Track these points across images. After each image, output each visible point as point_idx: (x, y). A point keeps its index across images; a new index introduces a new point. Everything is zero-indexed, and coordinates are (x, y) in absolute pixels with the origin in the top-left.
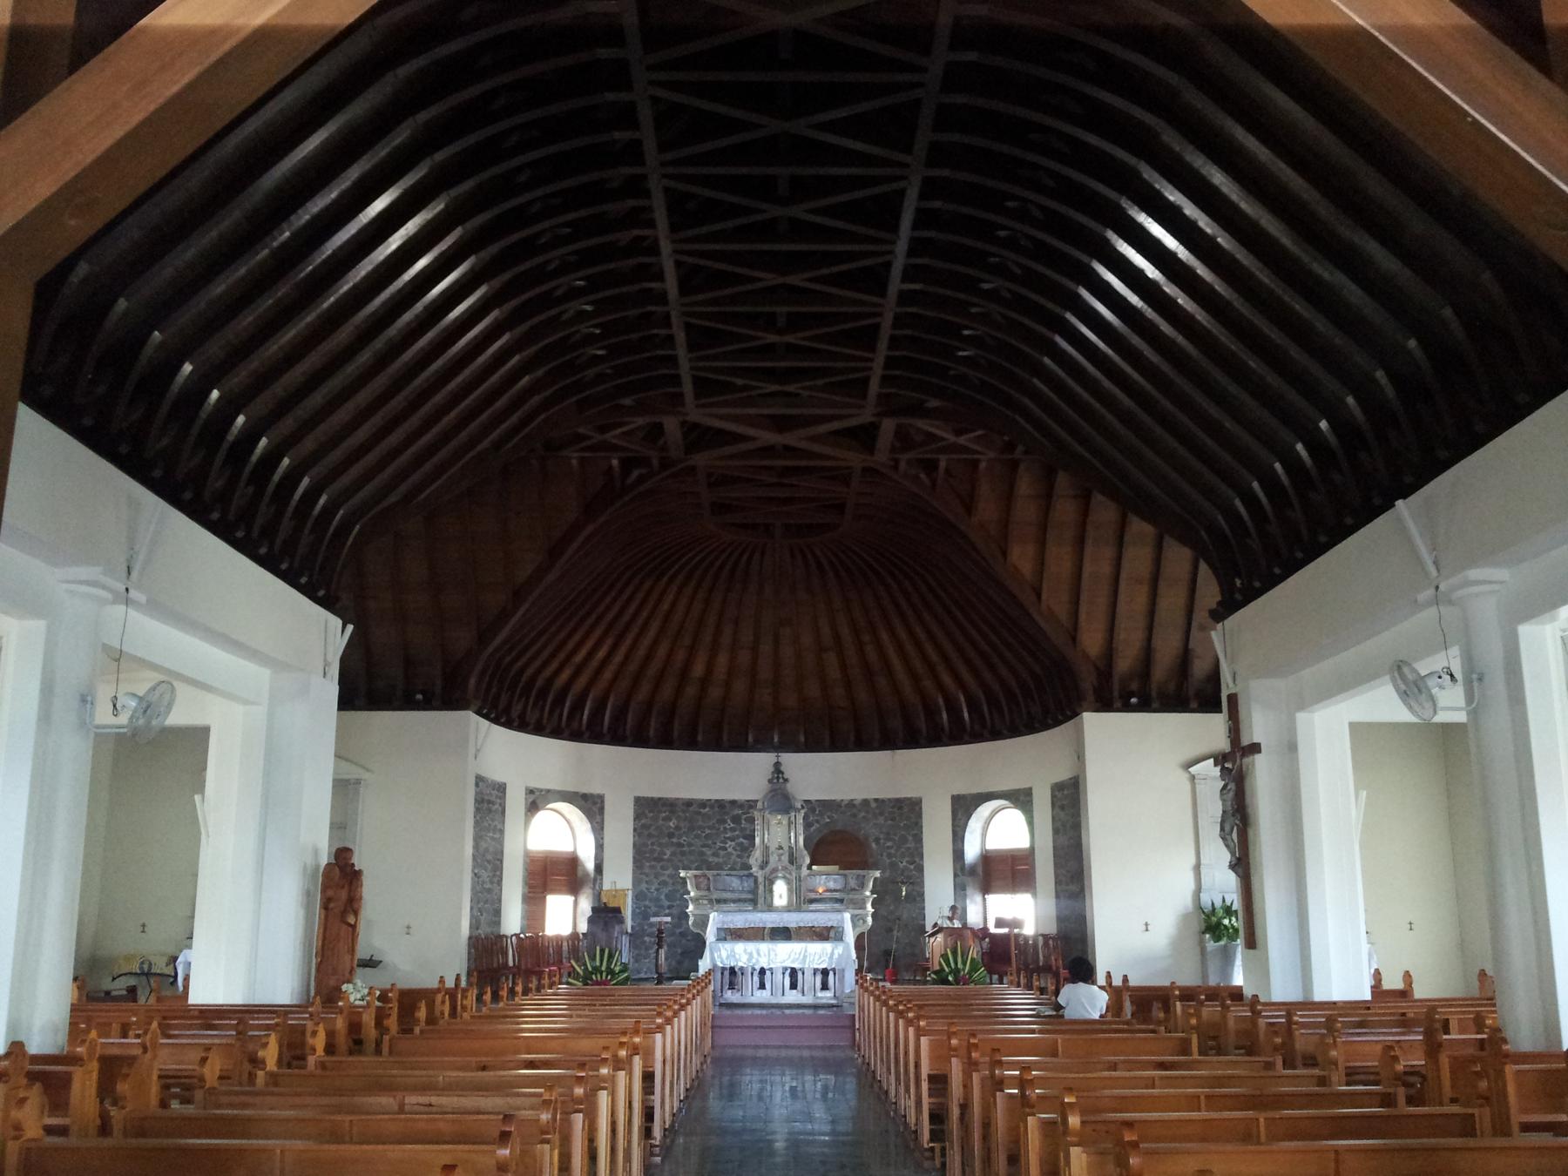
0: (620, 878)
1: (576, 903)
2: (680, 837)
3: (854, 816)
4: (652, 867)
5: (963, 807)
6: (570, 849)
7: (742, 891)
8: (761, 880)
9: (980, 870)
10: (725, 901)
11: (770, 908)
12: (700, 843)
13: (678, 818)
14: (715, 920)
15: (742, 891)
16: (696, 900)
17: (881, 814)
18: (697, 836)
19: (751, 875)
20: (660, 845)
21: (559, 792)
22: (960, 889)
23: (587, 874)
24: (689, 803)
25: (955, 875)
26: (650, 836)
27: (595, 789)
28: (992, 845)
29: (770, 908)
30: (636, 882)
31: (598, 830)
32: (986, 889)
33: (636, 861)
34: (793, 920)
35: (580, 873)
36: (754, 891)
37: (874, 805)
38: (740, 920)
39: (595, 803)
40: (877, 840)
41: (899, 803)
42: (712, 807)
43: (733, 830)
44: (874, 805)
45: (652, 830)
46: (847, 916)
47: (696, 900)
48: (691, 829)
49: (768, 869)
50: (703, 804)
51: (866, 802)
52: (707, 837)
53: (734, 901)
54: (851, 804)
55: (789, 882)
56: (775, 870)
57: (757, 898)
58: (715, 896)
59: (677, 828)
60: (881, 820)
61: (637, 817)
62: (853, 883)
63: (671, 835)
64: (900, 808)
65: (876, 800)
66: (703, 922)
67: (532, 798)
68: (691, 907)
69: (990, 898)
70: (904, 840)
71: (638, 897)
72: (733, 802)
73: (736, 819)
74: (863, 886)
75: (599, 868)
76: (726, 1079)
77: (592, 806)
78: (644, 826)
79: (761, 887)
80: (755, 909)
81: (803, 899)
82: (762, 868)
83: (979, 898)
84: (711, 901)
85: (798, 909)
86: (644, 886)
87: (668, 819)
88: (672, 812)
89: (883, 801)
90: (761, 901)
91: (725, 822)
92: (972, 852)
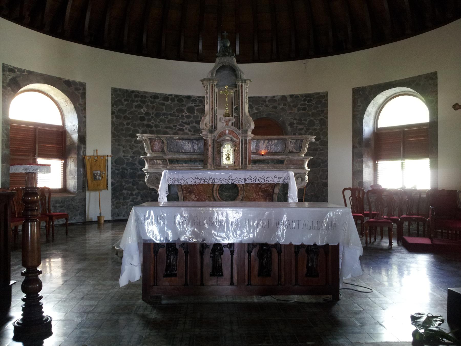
0: (101, 145)
1: (65, 166)
2: (149, 120)
3: (275, 107)
4: (127, 141)
5: (362, 97)
6: (60, 124)
7: (193, 153)
8: (210, 142)
9: (372, 143)
10: (178, 161)
11: (218, 166)
12: (164, 126)
13: (147, 106)
14: (166, 179)
15: (193, 153)
16: (150, 160)
17: (295, 106)
18: (161, 120)
19: (200, 139)
20: (134, 125)
21: (41, 75)
22: (358, 158)
23: (73, 143)
24: (155, 96)
25: (354, 147)
26: (125, 118)
27: (78, 79)
28: (382, 124)
29: (218, 166)
30: (114, 151)
31: (81, 111)
32: (377, 156)
33: (114, 135)
34: (240, 177)
35: (68, 143)
36: (204, 153)
37: (289, 100)
38: (189, 177)
39: (77, 89)
40: (291, 125)
41: (309, 97)
42: (173, 100)
43: (188, 117)
44: (289, 100)
45: (127, 114)
46: (292, 174)
47: (150, 160)
48: (157, 115)
49: (216, 133)
50: (166, 98)
51: (284, 98)
52: (170, 122)
53: (185, 161)
54: (273, 99)
55: (235, 145)
56: (223, 134)
57: (207, 157)
58: (170, 156)
59: (147, 114)
60: (295, 110)
61: (114, 104)
62: (291, 147)
63: (142, 119)
64: (310, 101)
65: (291, 96)
66: (156, 179)
67: (11, 76)
68: (147, 166)
69: (381, 164)
70: (312, 123)
71: (116, 162)
72: (189, 97)
73: (191, 110)
74: (300, 149)
75: (82, 138)
76: (211, 84)
77: (75, 92)
78: (120, 110)
79: (210, 149)
80: (205, 167)
81: (244, 161)
82: (211, 132)
83: (371, 164)
84: (164, 161)
85: (244, 168)
86: (121, 154)
87: (139, 107)
88: (144, 102)
89: (297, 97)
90: (210, 160)
91: (182, 111)
92: (367, 128)
